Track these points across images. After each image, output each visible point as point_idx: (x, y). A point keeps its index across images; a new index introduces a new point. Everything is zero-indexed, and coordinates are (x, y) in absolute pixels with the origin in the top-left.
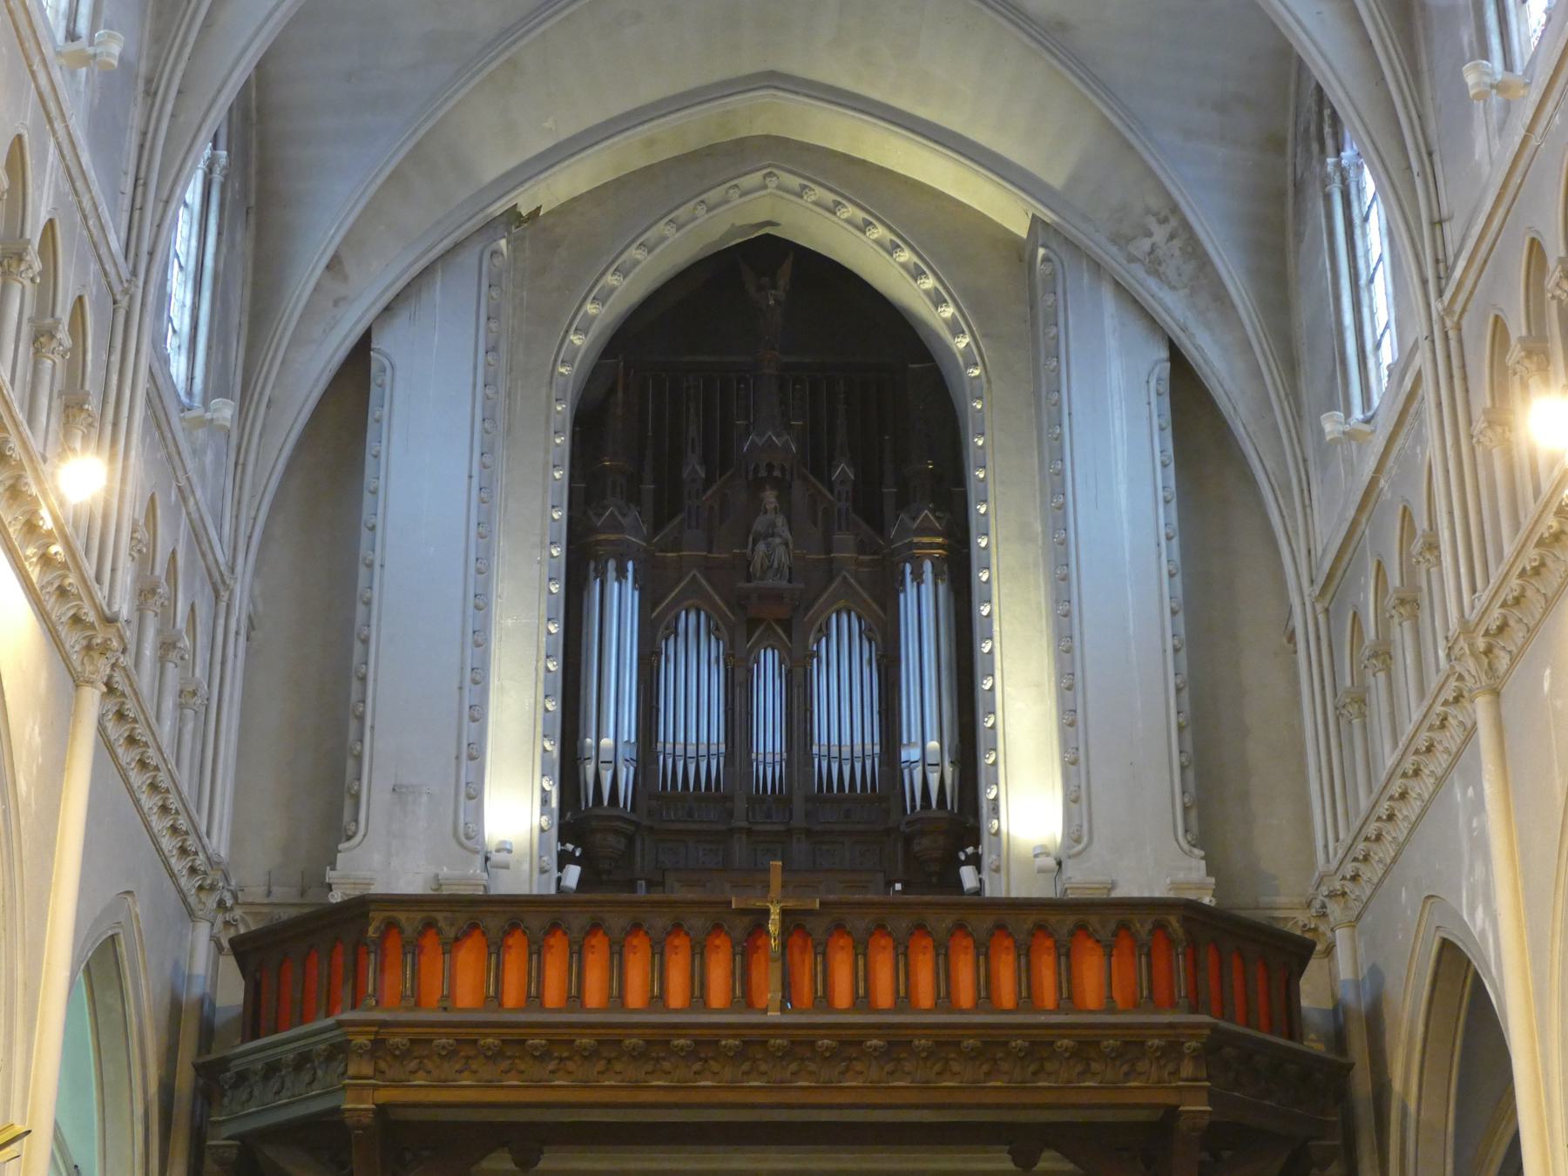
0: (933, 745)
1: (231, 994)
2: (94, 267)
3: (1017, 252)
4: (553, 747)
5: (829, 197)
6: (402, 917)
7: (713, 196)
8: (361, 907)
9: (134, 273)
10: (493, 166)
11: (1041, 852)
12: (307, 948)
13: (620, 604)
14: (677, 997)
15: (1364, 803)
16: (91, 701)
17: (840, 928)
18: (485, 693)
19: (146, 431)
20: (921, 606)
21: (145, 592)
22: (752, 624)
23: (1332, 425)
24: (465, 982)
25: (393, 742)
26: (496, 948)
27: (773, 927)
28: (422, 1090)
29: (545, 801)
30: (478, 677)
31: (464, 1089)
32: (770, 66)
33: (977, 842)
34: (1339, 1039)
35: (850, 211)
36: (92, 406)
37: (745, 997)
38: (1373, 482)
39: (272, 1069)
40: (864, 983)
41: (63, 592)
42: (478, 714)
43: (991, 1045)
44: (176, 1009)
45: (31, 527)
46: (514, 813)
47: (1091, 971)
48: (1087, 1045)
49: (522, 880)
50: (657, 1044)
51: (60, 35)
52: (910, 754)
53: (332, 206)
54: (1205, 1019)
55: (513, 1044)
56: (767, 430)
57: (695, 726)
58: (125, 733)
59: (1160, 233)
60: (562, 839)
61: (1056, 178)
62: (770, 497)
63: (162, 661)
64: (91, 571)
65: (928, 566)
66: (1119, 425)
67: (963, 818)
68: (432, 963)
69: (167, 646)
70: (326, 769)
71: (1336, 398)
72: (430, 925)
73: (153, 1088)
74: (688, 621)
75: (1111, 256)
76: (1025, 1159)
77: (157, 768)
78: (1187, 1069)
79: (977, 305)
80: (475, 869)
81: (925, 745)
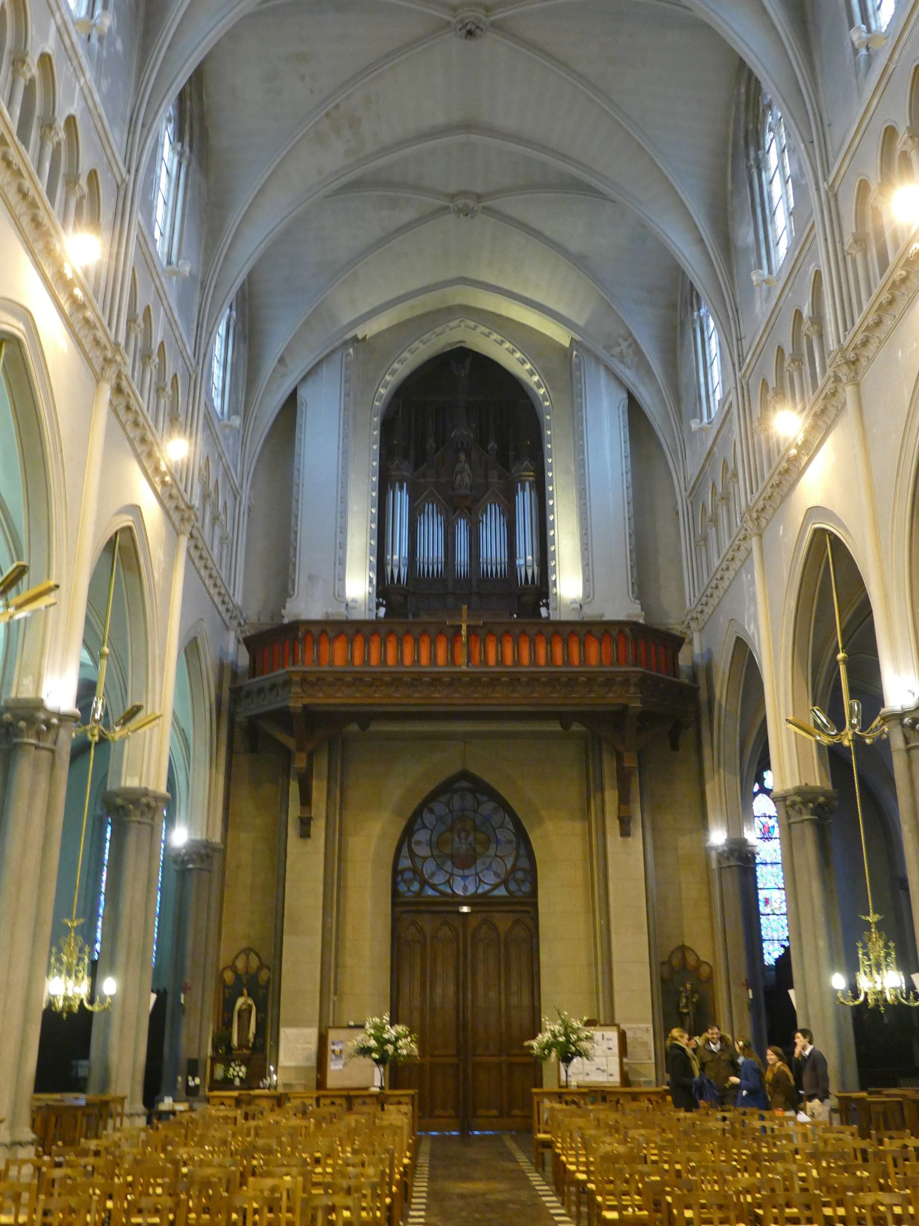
0: (529, 558)
1: (244, 660)
2: (180, 361)
4: (374, 559)
7: (438, 330)
8: (296, 625)
9: (198, 363)
10: (347, 317)
12: (275, 641)
13: (401, 500)
15: (706, 581)
16: (184, 541)
20: (524, 500)
24: (338, 656)
26: (351, 642)
27: (464, 632)
28: (321, 699)
33: (547, 597)
34: (694, 677)
35: (495, 336)
36: (182, 419)
38: (712, 448)
40: (501, 655)
41: (171, 496)
42: (343, 546)
44: (221, 666)
45: (157, 469)
46: (358, 586)
47: (593, 651)
48: (591, 680)
49: (362, 613)
50: (416, 680)
51: (165, 263)
52: (520, 562)
53: (279, 338)
55: (358, 680)
56: (461, 429)
57: (432, 550)
58: (198, 555)
59: (624, 345)
60: (378, 597)
61: (581, 322)
62: (462, 457)
65: (527, 484)
68: (325, 648)
69: (215, 518)
72: (324, 632)
74: (429, 508)
76: (566, 727)
79: (548, 376)
80: (342, 609)
81: (526, 559)
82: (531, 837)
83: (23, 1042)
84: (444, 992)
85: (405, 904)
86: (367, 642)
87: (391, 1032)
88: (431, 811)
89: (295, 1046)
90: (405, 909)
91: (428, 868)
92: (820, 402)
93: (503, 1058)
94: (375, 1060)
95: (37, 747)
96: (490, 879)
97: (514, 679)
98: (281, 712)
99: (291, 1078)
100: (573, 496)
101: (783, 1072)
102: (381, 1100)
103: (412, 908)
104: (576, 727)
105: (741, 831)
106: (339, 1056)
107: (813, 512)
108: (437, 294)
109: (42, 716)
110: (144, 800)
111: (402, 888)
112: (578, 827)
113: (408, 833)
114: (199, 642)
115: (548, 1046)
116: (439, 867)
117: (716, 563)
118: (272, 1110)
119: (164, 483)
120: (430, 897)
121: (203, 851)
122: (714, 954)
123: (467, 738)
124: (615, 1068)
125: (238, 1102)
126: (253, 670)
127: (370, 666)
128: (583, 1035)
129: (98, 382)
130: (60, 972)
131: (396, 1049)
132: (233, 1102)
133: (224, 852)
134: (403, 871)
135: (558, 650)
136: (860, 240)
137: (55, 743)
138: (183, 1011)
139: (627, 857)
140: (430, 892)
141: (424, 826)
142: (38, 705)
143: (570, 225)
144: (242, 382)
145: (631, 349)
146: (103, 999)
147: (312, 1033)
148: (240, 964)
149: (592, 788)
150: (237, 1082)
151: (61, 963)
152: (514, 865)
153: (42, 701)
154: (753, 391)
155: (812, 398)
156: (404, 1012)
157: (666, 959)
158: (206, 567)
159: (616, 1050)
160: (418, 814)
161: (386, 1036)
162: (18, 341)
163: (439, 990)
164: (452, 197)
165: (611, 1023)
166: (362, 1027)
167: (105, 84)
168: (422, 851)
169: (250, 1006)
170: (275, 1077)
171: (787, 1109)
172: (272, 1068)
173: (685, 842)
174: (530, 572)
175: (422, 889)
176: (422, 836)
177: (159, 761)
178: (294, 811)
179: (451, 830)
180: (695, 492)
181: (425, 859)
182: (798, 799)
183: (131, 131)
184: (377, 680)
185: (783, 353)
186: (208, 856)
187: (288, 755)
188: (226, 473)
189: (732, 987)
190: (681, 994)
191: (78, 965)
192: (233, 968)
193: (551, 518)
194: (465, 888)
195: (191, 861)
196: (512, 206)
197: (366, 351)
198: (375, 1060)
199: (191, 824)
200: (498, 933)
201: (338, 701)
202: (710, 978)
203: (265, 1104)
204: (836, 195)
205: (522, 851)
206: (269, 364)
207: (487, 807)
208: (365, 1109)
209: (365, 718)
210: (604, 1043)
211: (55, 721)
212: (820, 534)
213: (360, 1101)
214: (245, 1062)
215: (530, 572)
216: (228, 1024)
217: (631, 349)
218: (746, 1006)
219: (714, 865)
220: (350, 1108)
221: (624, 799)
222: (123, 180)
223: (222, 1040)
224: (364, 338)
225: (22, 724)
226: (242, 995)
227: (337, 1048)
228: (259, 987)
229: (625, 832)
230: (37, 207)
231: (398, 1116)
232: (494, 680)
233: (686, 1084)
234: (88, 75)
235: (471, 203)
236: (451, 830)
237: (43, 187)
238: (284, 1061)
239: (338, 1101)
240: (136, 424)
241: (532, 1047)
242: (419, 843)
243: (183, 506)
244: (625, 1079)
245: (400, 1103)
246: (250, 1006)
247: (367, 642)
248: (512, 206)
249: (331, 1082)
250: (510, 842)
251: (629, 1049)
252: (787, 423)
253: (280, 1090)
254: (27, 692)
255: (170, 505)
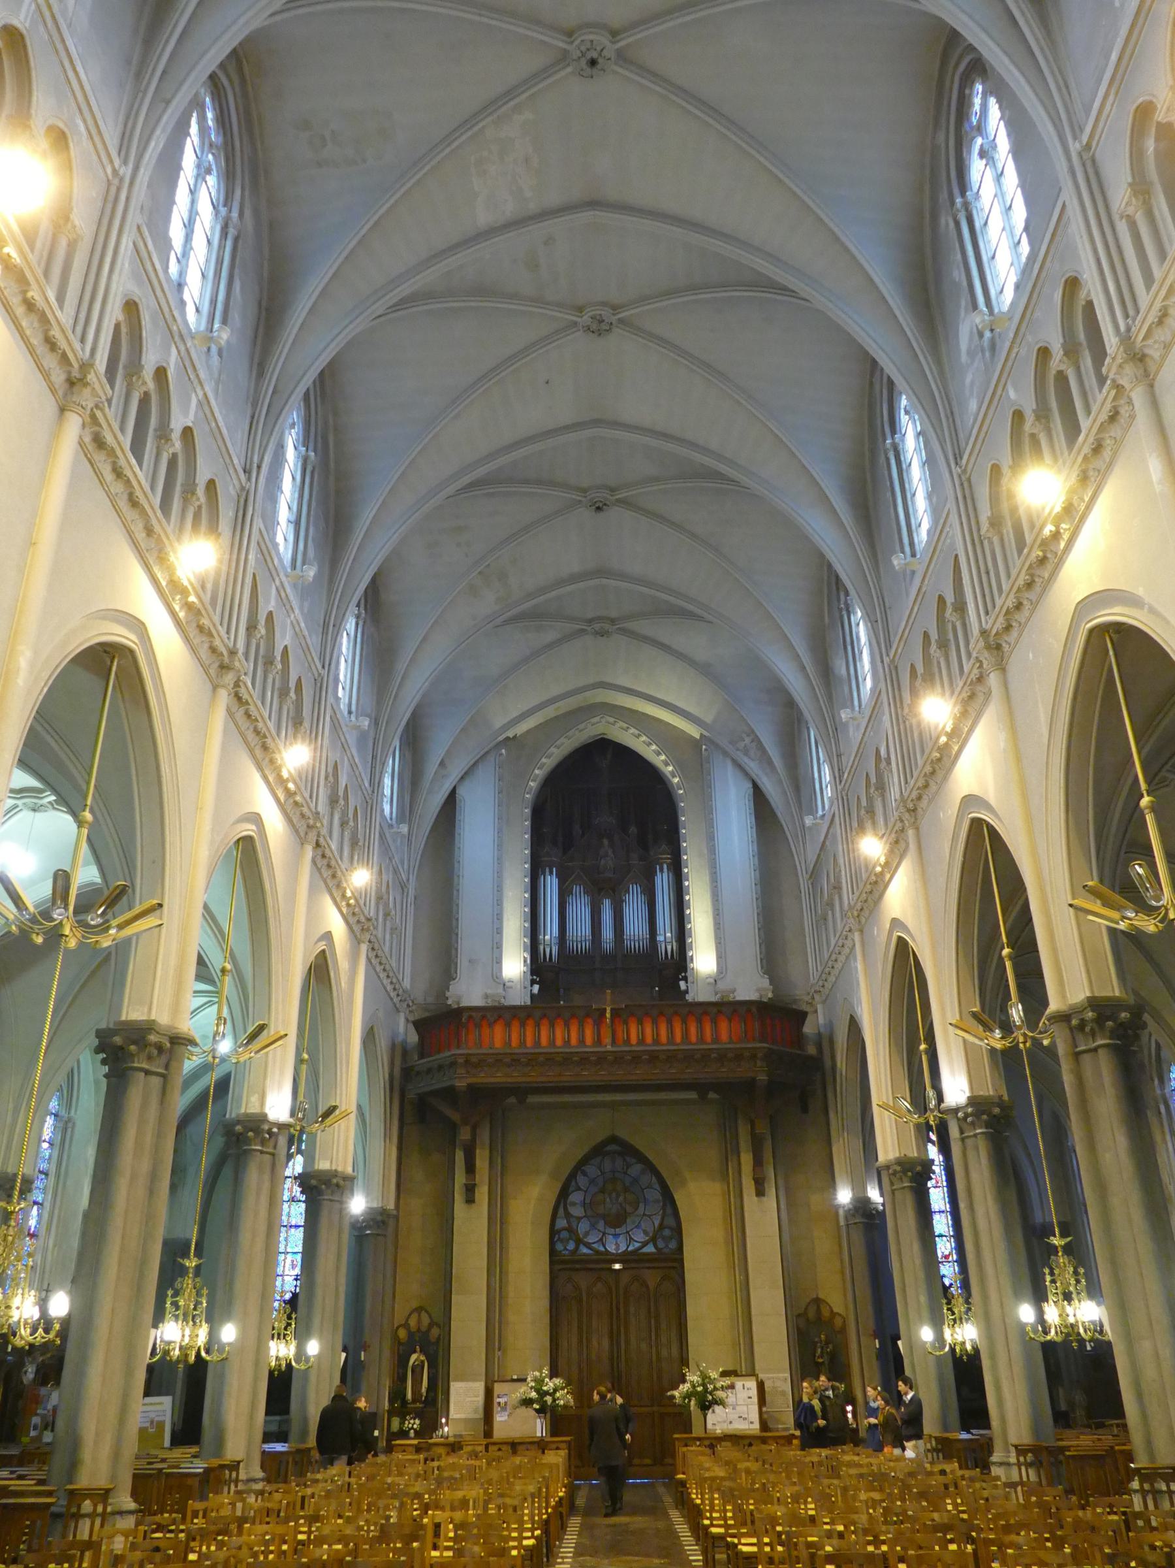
0: (669, 935)
1: (413, 1038)
2: (360, 793)
3: (696, 744)
4: (527, 941)
5: (625, 725)
6: (474, 1014)
7: (581, 726)
8: (460, 1011)
10: (498, 723)
11: (709, 977)
12: (441, 1024)
13: (551, 884)
14: (574, 1041)
15: (826, 957)
16: (364, 947)
17: (632, 1015)
18: (501, 923)
19: (380, 846)
20: (663, 880)
21: (333, 801)
22: (600, 890)
23: (808, 821)
24: (498, 1038)
25: (468, 945)
26: (508, 1025)
27: (608, 1015)
28: (483, 1078)
29: (525, 961)
30: (499, 917)
31: (499, 1077)
32: (598, 680)
33: (686, 971)
34: (819, 1046)
35: (632, 730)
36: (306, 724)
37: (598, 1041)
38: (824, 842)
39: (429, 1071)
40: (643, 1034)
41: (354, 914)
42: (499, 931)
43: (688, 1057)
44: (393, 1047)
45: (344, 896)
46: (514, 965)
47: (724, 1026)
48: (722, 1057)
49: (519, 997)
50: (566, 1060)
51: (346, 713)
52: (660, 938)
53: (439, 744)
54: (765, 1045)
55: (515, 1061)
56: (604, 815)
57: (580, 928)
58: (376, 958)
59: (747, 740)
60: (532, 974)
61: (708, 719)
62: (606, 842)
63: (385, 920)
64: (307, 795)
65: (665, 866)
66: (734, 813)
67: (681, 961)
68: (486, 1031)
69: (386, 915)
70: (444, 954)
71: (812, 811)
72: (484, 1017)
73: (387, 1076)
74: (576, 889)
75: (730, 749)
76: (703, 1097)
77: (247, 703)
78: (759, 1063)
79: (681, 766)
80: (500, 990)
81: (666, 935)
82: (676, 1197)
83: (255, 1394)
84: (601, 1344)
85: (563, 1262)
86: (523, 1025)
87: (549, 1385)
88: (585, 1174)
89: (464, 1399)
90: (561, 1267)
91: (583, 1227)
92: (893, 835)
93: (655, 1409)
94: (537, 1411)
95: (262, 1152)
96: (640, 1237)
97: (653, 1057)
98: (446, 1087)
99: (461, 1430)
100: (707, 878)
101: (892, 1414)
102: (541, 1446)
103: (568, 1266)
104: (712, 1095)
105: (865, 1190)
106: (504, 1409)
107: (970, 800)
108: (580, 697)
109: (266, 1127)
110: (335, 1181)
111: (559, 1247)
112: (717, 1187)
113: (564, 1194)
114: (375, 1029)
115: (688, 1396)
116: (593, 1226)
117: (833, 942)
118: (448, 1454)
119: (348, 905)
120: (584, 1254)
121: (379, 1218)
122: (847, 1308)
123: (613, 1106)
124: (754, 1416)
125: (418, 1449)
126: (424, 1048)
127: (526, 1047)
128: (719, 1385)
129: (62, 410)
130: (176, 1317)
131: (554, 1400)
132: (413, 1449)
133: (397, 1218)
134: (559, 1232)
135: (693, 1030)
136: (996, 522)
137: (275, 1147)
138: (364, 1367)
139: (763, 1216)
140: (585, 1250)
141: (579, 1189)
142: (263, 1118)
143: (695, 642)
144: (407, 783)
145: (754, 744)
146: (307, 1360)
147: (479, 1387)
148: (413, 1322)
149: (730, 1151)
150: (412, 1433)
151: (177, 1308)
152: (661, 1224)
153: (266, 1115)
154: (900, 682)
155: (961, 684)
156: (562, 1363)
157: (802, 1311)
158: (380, 963)
159: (755, 1399)
160: (572, 1176)
161: (545, 1388)
162: (131, 651)
163: (595, 1343)
164: (590, 621)
165: (752, 1373)
166: (524, 1380)
167: (306, 604)
168: (577, 1211)
169: (423, 1362)
170: (446, 1429)
171: (895, 1447)
172: (444, 1420)
173: (815, 1199)
174: (669, 948)
175: (577, 1248)
176: (576, 1197)
177: (346, 1147)
178: (460, 1178)
179: (602, 1191)
180: (814, 875)
181: (579, 1219)
182: (898, 1168)
183: (325, 632)
184: (532, 1060)
185: (945, 602)
186: (383, 1222)
187: (453, 1128)
188: (396, 871)
189: (862, 1339)
190: (816, 1344)
191: (286, 1329)
192: (406, 1325)
193: (687, 898)
194: (617, 1245)
195: (366, 1228)
196: (643, 627)
197: (515, 748)
198: (537, 1411)
199: (368, 1194)
200: (647, 1287)
201: (498, 1080)
202: (843, 1330)
203: (441, 1451)
204: (896, 668)
205: (669, 1211)
206: (431, 767)
207: (636, 1169)
208: (527, 1453)
209: (521, 1092)
210: (746, 1389)
211: (275, 1130)
212: (977, 824)
213: (523, 1447)
214: (418, 1414)
215: (669, 948)
216: (403, 1379)
217: (754, 744)
218: (874, 1357)
219: (842, 1222)
220: (515, 1452)
221: (758, 1163)
222: (319, 674)
223: (397, 1395)
224: (515, 737)
225: (251, 1134)
226: (415, 1352)
227: (502, 1400)
228: (429, 1344)
229: (760, 1193)
230: (212, 636)
231: (556, 1458)
232: (636, 1058)
233: (820, 1430)
234: (297, 611)
235: (607, 626)
236: (602, 1191)
237: (127, 442)
238: (454, 1413)
239: (504, 1448)
240: (329, 866)
241: (673, 1397)
242: (574, 1204)
243: (363, 919)
244: (764, 1426)
245: (558, 1448)
246: (423, 1362)
247: (523, 1025)
248: (643, 627)
249: (499, 1433)
250: (657, 1201)
251: (768, 1398)
252: (935, 710)
253: (451, 1439)
254: (253, 1109)
255: (352, 920)
